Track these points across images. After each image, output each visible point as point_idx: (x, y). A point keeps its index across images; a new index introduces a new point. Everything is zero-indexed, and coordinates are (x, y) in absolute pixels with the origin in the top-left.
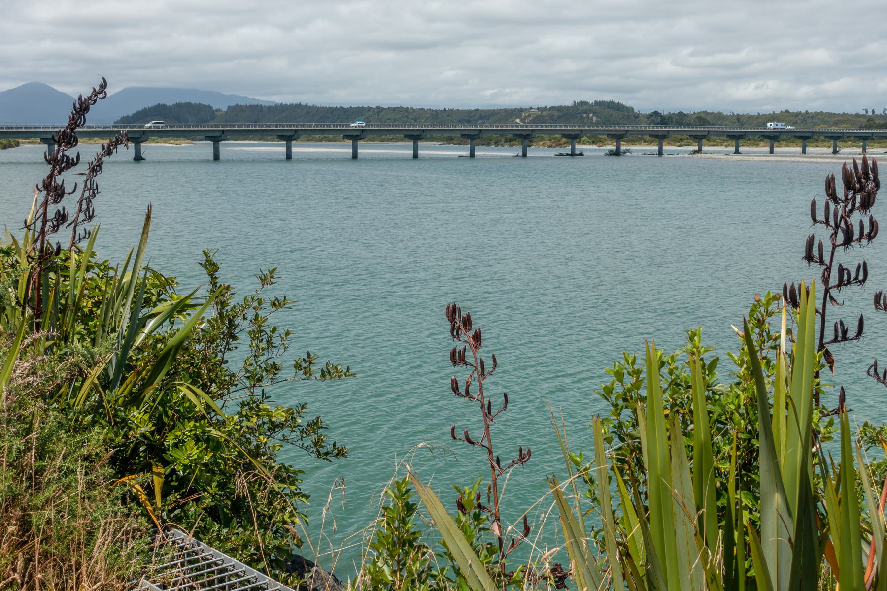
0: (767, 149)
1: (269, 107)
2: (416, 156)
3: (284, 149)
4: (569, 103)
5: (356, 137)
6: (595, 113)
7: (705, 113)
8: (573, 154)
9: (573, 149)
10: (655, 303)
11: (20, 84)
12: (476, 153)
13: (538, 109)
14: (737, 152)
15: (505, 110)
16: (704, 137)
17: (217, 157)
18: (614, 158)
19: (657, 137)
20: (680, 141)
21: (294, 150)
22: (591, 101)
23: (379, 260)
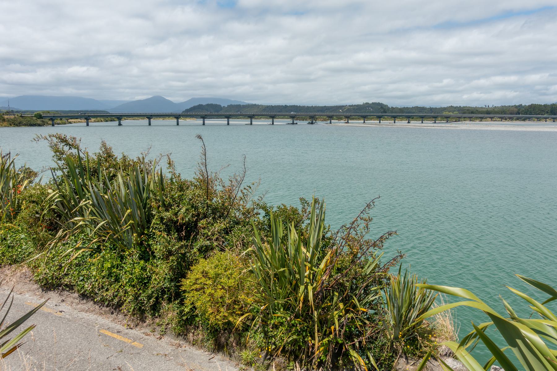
0: (363, 121)
1: (243, 106)
2: (228, 124)
3: (202, 122)
4: (362, 104)
5: (251, 117)
6: (372, 108)
7: (554, 104)
8: (293, 124)
9: (293, 122)
10: (457, 227)
11: (150, 97)
12: (253, 123)
13: (349, 106)
14: (409, 123)
15: (336, 106)
16: (449, 117)
17: (178, 124)
18: (311, 125)
19: (363, 117)
20: (386, 119)
21: (206, 122)
22: (370, 102)
23: (535, 257)
